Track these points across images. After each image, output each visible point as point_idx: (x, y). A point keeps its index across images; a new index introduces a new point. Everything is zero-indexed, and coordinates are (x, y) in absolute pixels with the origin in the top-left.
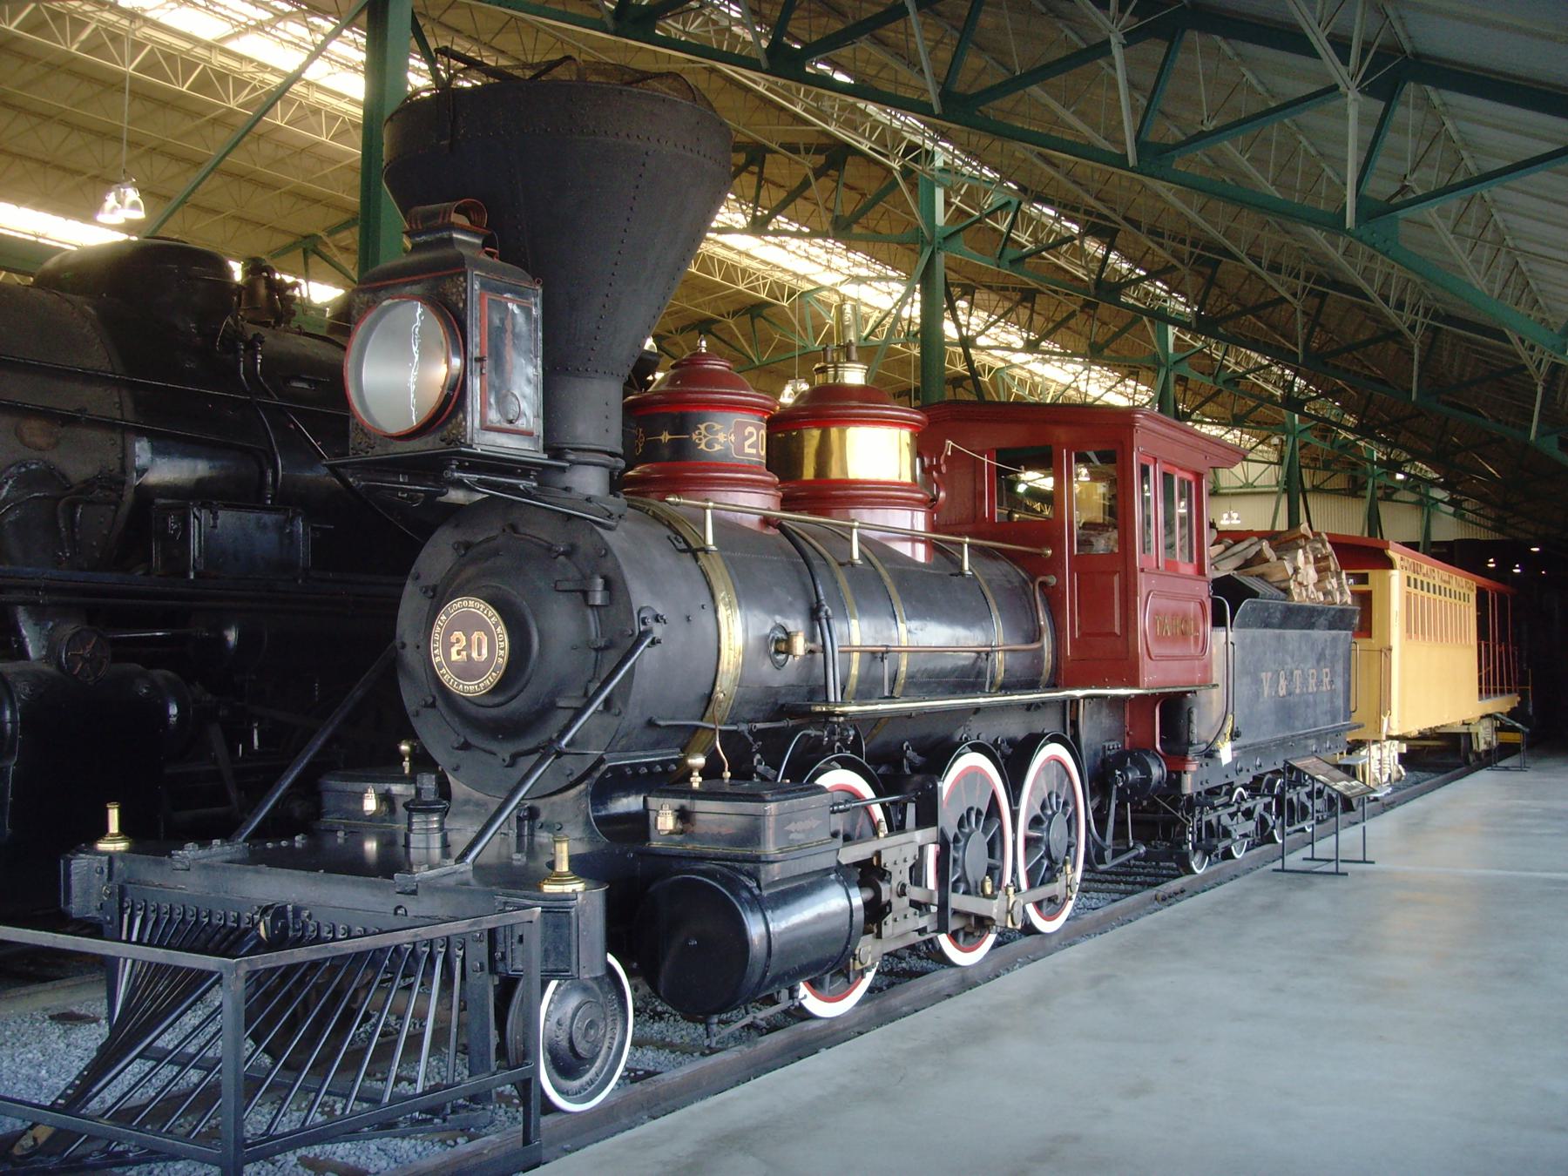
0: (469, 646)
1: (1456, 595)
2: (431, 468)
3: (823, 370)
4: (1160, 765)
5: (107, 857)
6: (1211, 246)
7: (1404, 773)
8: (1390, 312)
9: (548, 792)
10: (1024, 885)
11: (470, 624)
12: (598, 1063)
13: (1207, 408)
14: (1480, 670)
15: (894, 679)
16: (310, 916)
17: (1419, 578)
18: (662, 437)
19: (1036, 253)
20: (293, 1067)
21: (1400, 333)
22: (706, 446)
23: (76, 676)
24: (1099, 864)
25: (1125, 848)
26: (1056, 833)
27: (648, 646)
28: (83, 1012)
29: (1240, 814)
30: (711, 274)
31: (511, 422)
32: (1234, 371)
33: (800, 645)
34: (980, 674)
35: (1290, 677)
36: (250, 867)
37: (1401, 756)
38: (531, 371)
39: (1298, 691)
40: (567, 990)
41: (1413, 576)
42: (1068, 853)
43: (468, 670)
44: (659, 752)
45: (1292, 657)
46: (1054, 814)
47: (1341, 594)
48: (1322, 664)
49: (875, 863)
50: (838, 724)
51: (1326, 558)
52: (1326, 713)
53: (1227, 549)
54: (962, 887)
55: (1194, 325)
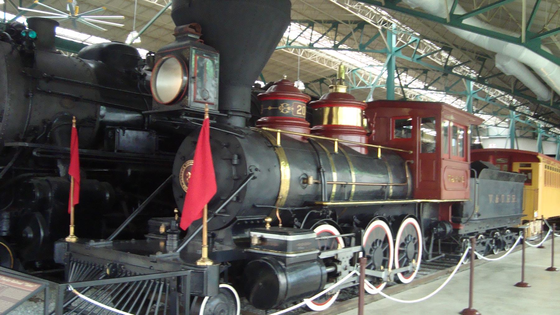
2: (176, 114)
13: (485, 109)
15: (350, 193)
16: (124, 268)
26: (410, 248)
27: (252, 179)
31: (205, 100)
33: (311, 181)
35: (500, 197)
38: (214, 82)
39: (502, 202)
44: (259, 216)
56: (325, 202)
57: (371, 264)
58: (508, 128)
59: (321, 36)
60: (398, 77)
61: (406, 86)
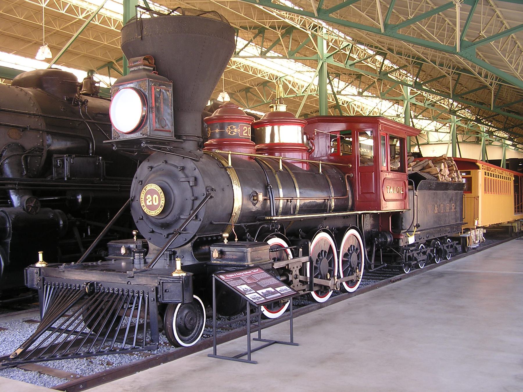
0: (152, 200)
1: (505, 178)
3: (272, 107)
4: (391, 237)
5: (39, 269)
6: (419, 58)
7: (485, 240)
8: (482, 79)
9: (179, 246)
10: (342, 276)
11: (152, 192)
12: (194, 331)
13: (424, 114)
14: (515, 205)
15: (295, 206)
16: (101, 285)
17: (490, 172)
18: (216, 131)
19: (360, 62)
20: (103, 334)
21: (486, 86)
22: (230, 133)
23: (29, 212)
24: (369, 269)
25: (380, 264)
26: (354, 258)
27: (209, 198)
28: (35, 320)
29: (421, 253)
30: (229, 78)
31: (163, 127)
32: (432, 101)
33: (261, 197)
34: (326, 206)
36: (83, 270)
37: (484, 233)
40: (184, 308)
41: (487, 172)
42: (358, 265)
43: (152, 207)
45: (440, 200)
46: (352, 252)
47: (458, 178)
48: (452, 202)
49: (287, 268)
50: (275, 223)
51: (452, 166)
52: (453, 219)
53: (417, 163)
54: (319, 276)
55: (414, 86)
56: (274, 216)
57: (318, 274)
58: (449, 133)
59: (247, 42)
60: (330, 83)
61: (339, 93)
